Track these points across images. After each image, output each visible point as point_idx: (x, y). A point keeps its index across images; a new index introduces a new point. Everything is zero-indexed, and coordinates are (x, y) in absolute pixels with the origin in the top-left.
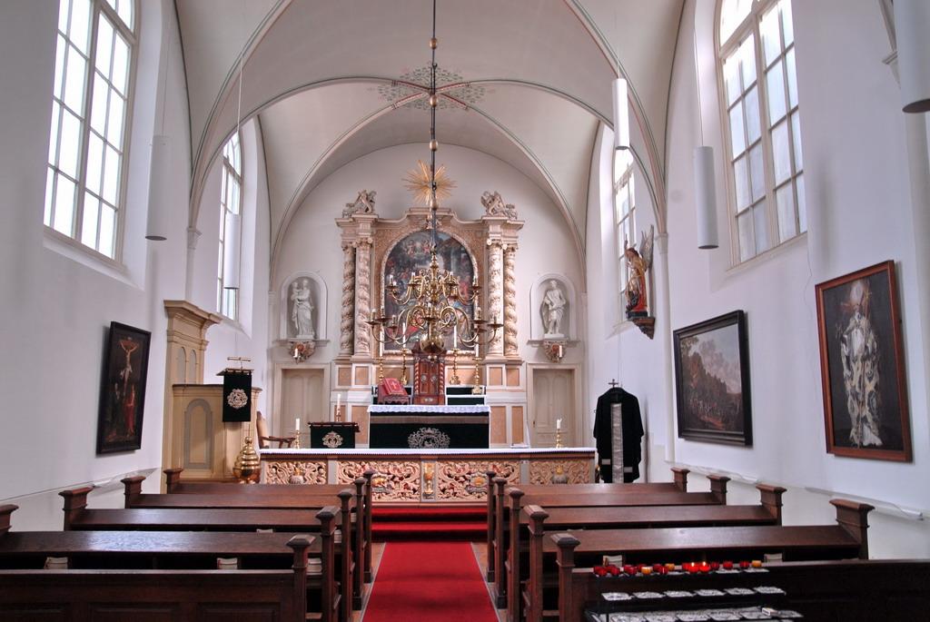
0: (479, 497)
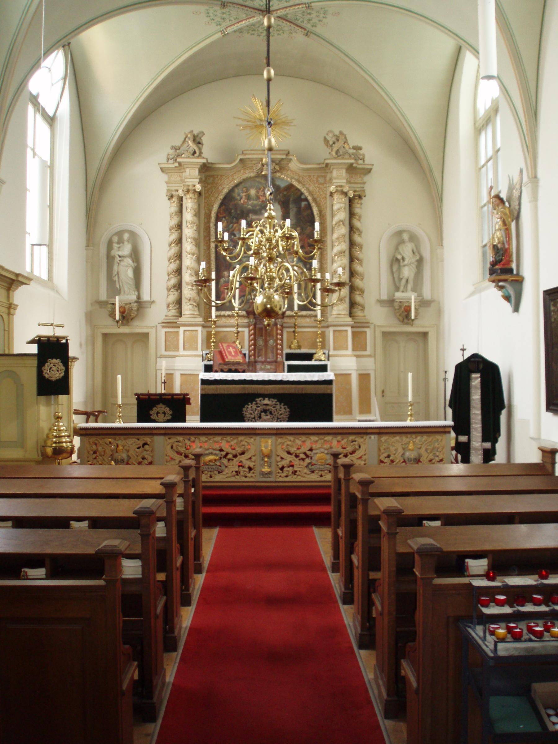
0: (321, 476)
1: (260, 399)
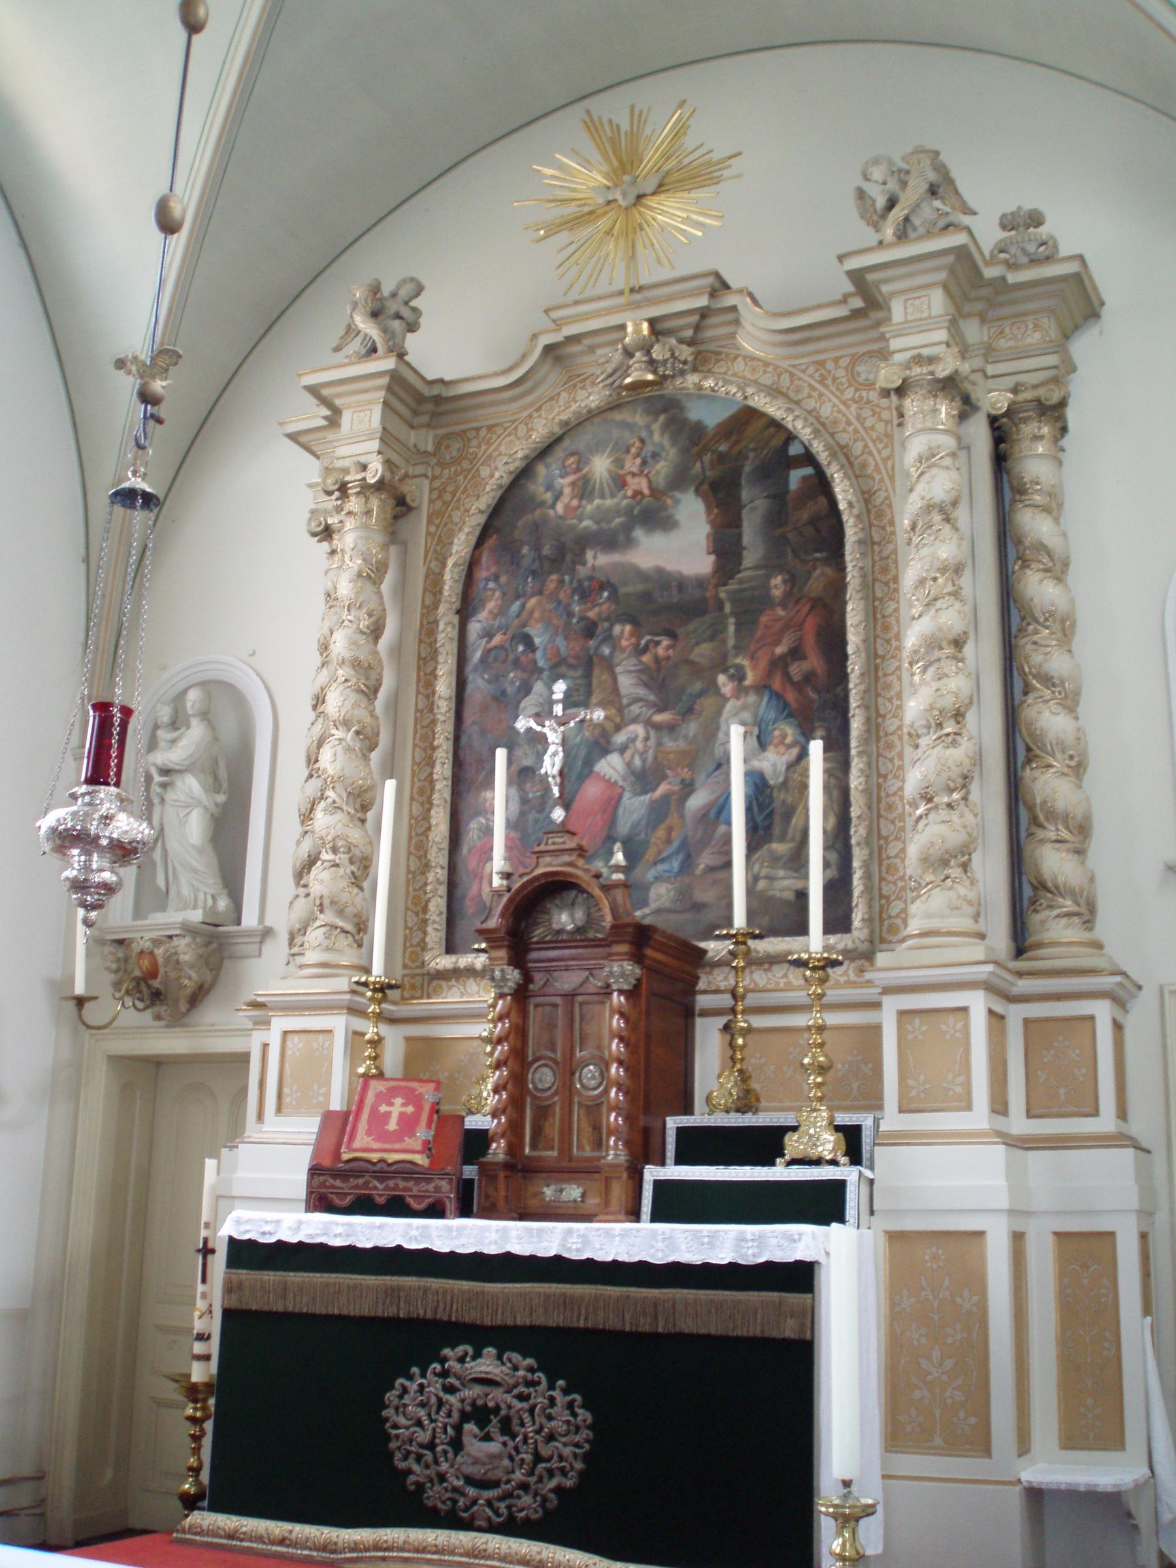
1: (460, 1349)
